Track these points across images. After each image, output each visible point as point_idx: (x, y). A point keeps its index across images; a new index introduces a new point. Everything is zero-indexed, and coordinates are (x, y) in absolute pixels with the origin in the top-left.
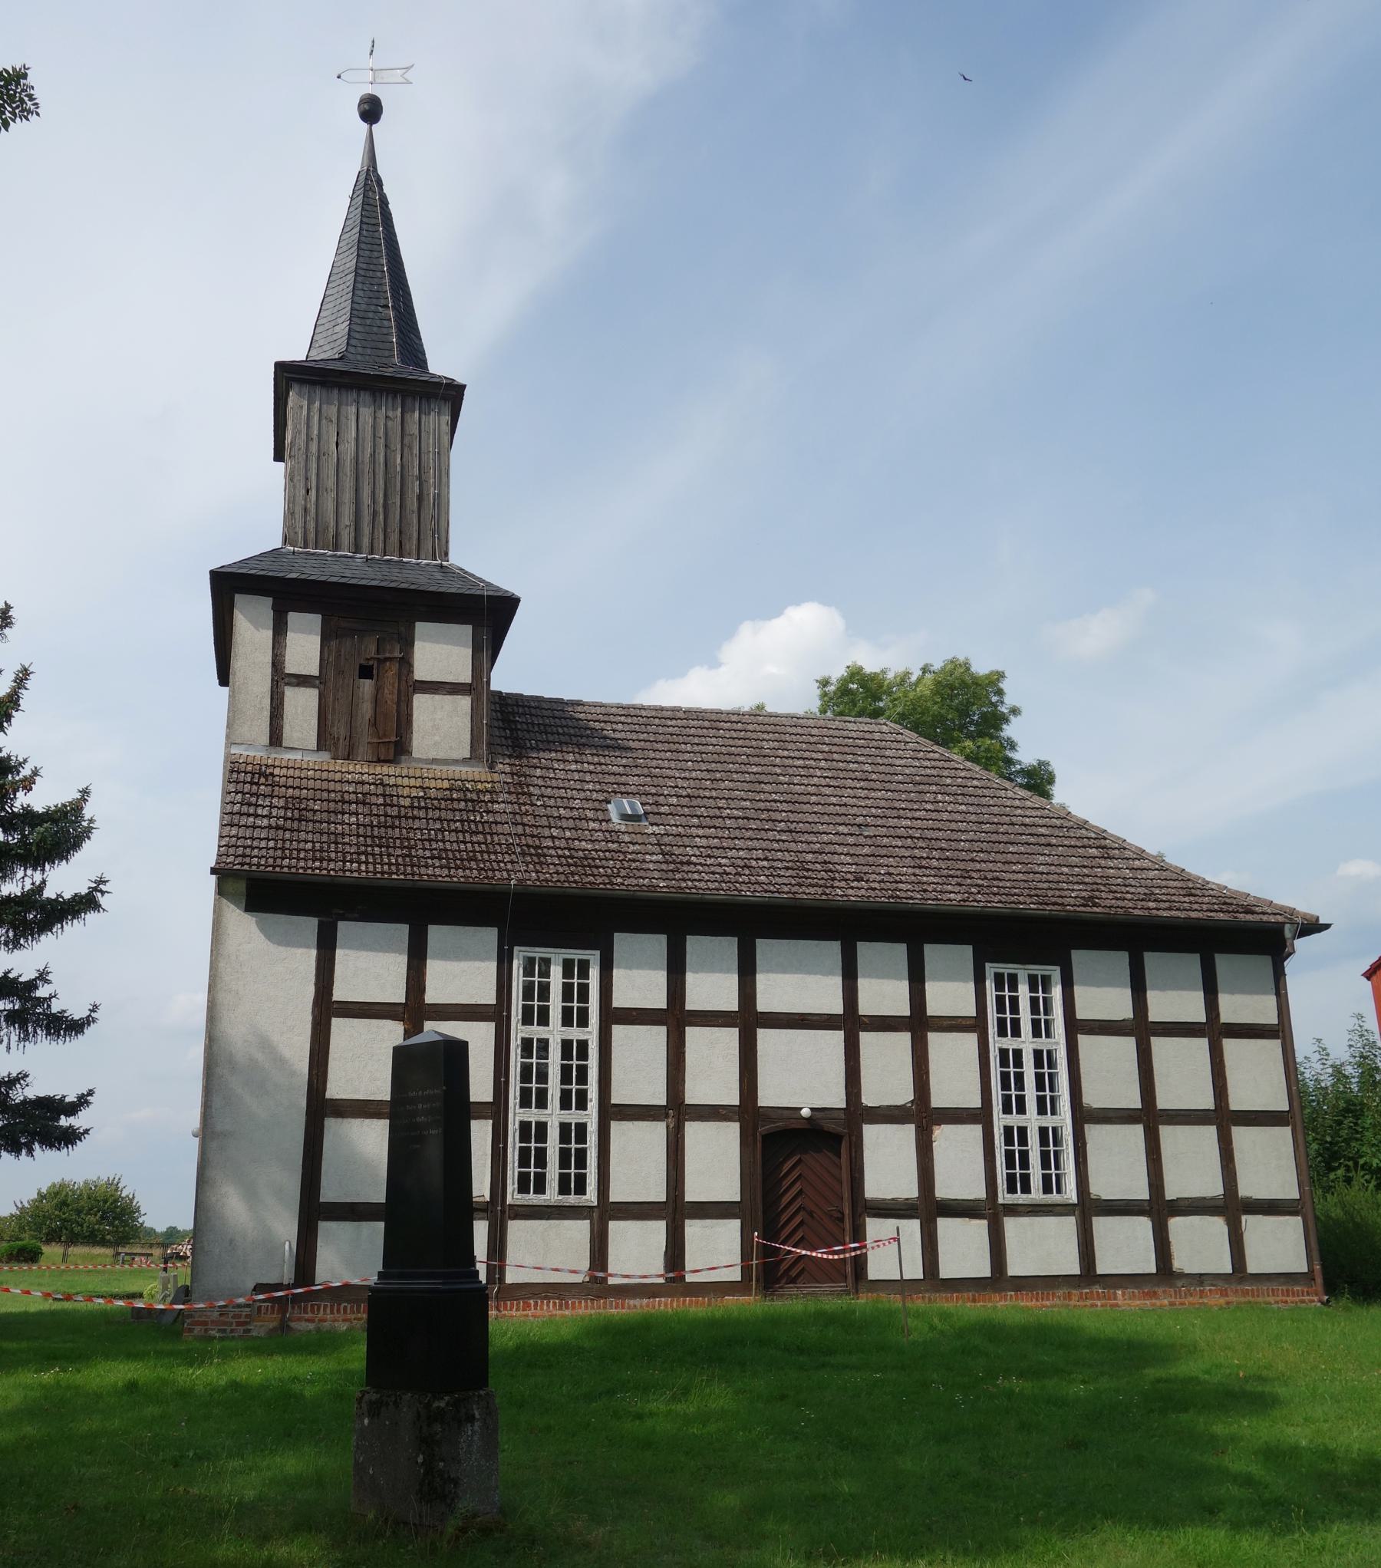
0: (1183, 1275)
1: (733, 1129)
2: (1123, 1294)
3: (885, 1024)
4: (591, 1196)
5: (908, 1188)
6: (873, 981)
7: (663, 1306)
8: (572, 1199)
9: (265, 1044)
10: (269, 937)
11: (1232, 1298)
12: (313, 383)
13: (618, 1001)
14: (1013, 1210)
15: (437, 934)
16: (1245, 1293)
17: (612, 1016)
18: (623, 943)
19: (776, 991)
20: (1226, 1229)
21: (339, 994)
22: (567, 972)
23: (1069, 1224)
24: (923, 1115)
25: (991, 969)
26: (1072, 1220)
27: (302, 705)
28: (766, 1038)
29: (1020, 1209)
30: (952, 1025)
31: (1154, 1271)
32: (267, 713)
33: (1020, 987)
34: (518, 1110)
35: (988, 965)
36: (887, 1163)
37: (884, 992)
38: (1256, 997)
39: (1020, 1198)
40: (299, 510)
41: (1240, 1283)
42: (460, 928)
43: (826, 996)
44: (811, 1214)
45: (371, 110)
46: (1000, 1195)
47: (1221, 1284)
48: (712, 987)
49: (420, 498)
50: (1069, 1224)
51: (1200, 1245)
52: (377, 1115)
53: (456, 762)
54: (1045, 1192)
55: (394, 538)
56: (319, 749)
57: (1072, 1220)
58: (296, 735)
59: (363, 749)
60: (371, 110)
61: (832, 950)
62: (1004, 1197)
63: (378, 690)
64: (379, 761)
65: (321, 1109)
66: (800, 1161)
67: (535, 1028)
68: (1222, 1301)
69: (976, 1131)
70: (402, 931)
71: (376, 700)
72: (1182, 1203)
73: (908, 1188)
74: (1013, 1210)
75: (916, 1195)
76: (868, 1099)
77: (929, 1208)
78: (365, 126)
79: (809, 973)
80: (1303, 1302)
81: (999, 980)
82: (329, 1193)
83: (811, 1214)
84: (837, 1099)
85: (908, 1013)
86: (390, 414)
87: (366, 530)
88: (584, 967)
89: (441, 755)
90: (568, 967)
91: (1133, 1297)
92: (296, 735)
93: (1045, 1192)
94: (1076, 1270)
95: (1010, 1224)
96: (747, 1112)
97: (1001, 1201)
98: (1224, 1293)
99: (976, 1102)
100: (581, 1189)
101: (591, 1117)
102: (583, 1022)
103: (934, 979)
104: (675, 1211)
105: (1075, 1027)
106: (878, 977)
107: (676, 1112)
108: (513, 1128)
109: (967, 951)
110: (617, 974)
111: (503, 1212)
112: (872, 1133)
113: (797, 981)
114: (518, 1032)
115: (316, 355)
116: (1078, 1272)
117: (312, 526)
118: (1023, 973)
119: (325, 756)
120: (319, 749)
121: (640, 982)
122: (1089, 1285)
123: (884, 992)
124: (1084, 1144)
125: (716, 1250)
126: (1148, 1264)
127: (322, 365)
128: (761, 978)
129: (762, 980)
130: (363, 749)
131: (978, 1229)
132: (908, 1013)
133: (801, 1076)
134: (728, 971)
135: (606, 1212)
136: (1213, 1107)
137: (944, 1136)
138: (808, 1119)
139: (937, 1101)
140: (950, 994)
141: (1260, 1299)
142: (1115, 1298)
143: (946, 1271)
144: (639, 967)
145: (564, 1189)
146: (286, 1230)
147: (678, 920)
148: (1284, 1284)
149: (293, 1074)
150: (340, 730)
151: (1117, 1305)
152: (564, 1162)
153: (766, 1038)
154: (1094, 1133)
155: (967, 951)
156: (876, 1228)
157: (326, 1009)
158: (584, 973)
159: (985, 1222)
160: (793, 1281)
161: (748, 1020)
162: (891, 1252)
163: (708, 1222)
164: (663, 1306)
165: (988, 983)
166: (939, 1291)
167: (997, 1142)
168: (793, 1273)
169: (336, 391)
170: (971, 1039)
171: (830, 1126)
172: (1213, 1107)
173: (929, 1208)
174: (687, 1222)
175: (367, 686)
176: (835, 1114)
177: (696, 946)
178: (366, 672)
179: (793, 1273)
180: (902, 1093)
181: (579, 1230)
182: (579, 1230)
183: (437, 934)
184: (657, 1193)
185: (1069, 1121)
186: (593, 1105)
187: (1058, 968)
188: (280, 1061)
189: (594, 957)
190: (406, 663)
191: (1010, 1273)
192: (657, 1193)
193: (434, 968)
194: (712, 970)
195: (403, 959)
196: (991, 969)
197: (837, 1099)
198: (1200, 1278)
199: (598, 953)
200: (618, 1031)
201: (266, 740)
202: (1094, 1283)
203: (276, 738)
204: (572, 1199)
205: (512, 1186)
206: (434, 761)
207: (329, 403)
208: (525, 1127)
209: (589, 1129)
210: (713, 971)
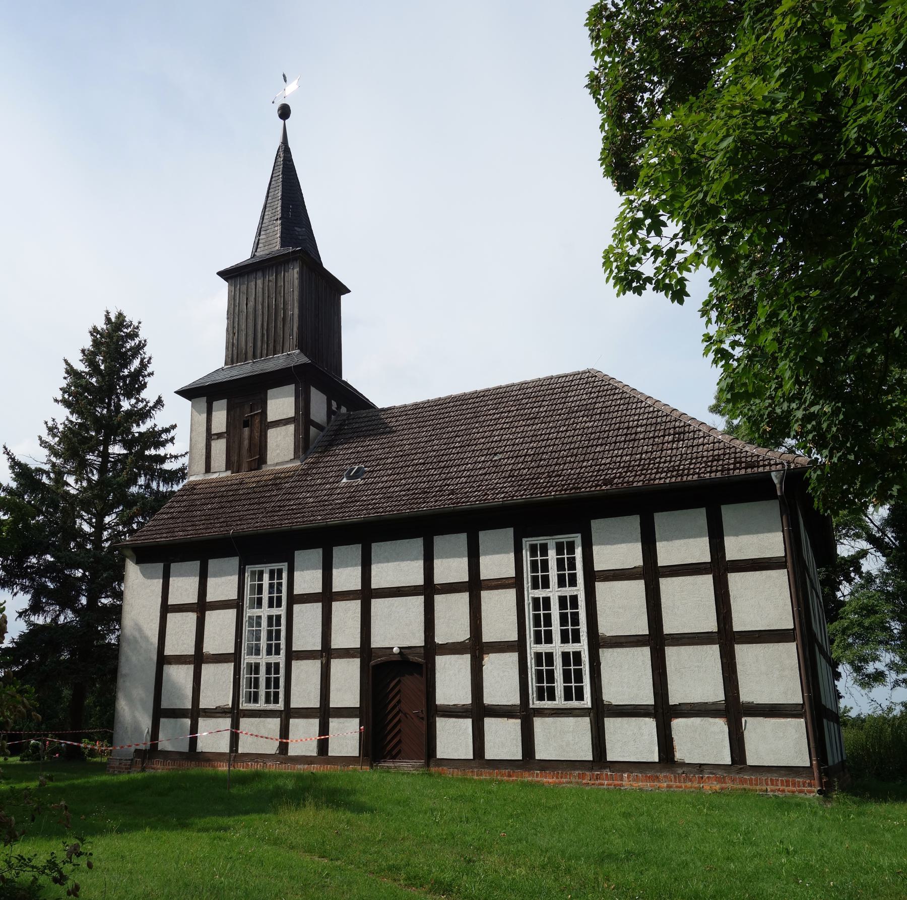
0: (683, 764)
1: (357, 662)
2: (628, 777)
3: (452, 588)
4: (280, 706)
5: (464, 697)
6: (444, 560)
7: (315, 768)
8: (574, 704)
9: (140, 630)
10: (144, 575)
11: (729, 785)
12: (236, 276)
13: (297, 591)
14: (542, 713)
15: (660, 519)
16: (743, 781)
17: (294, 600)
18: (300, 556)
19: (385, 574)
20: (726, 729)
21: (171, 601)
22: (559, 551)
23: (585, 723)
24: (476, 648)
25: (527, 542)
26: (587, 720)
27: (219, 448)
28: (735, 580)
29: (546, 712)
30: (499, 584)
31: (657, 760)
32: (204, 457)
33: (550, 552)
34: (532, 645)
35: (524, 540)
36: (452, 681)
37: (451, 568)
38: (761, 536)
39: (547, 704)
40: (230, 346)
41: (738, 773)
42: (618, 519)
43: (697, 550)
44: (405, 714)
45: (285, 112)
46: (531, 702)
47: (720, 773)
48: (347, 577)
49: (284, 319)
50: (585, 722)
51: (702, 742)
52: (353, 657)
53: (287, 462)
54: (566, 700)
55: (271, 346)
56: (227, 470)
57: (587, 720)
58: (216, 465)
59: (245, 466)
60: (285, 112)
61: (634, 523)
62: (280, 706)
63: (251, 431)
64: (251, 470)
65: (163, 660)
66: (399, 681)
67: (255, 610)
68: (717, 787)
69: (514, 657)
70: (463, 538)
71: (251, 438)
72: (684, 708)
73: (464, 697)
74: (542, 713)
75: (470, 702)
76: (439, 639)
77: (478, 711)
78: (282, 121)
79: (403, 560)
80: (801, 792)
81: (533, 550)
82: (165, 705)
83: (405, 714)
84: (417, 639)
85: (467, 579)
86: (271, 278)
87: (259, 343)
88: (571, 548)
89: (280, 460)
90: (559, 549)
91: (636, 779)
92: (216, 465)
93: (566, 700)
94: (519, 756)
95: (539, 724)
96: (365, 652)
97: (531, 706)
98: (721, 780)
99: (514, 637)
100: (580, 697)
101: (281, 659)
102: (573, 583)
103: (486, 554)
104: (325, 713)
105: (592, 577)
106: (447, 557)
107: (327, 653)
108: (243, 666)
109: (510, 531)
110: (297, 574)
111: (238, 713)
112: (441, 661)
113: (397, 568)
114: (531, 594)
115: (262, 252)
116: (591, 759)
117: (235, 352)
118: (551, 543)
119: (229, 473)
120: (227, 470)
121: (308, 580)
122: (740, 771)
123: (451, 568)
124: (599, 664)
125: (346, 737)
126: (467, 753)
127: (268, 257)
128: (596, 549)
129: (438, 563)
130: (245, 466)
131: (514, 726)
132: (467, 579)
133: (397, 627)
134: (507, 552)
135: (288, 714)
136: (716, 630)
137: (491, 662)
138: (400, 653)
139: (487, 637)
140: (497, 563)
141: (758, 787)
142: (622, 780)
143: (489, 754)
144: (308, 569)
145: (568, 697)
146: (146, 723)
147: (326, 539)
148: (785, 775)
149: (152, 644)
150: (235, 458)
151: (621, 785)
152: (567, 678)
153: (735, 580)
154: (607, 656)
155: (510, 531)
156: (442, 724)
157: (166, 609)
158: (571, 550)
159: (519, 721)
160: (394, 757)
161: (719, 568)
162: (453, 739)
163: (342, 720)
164: (315, 768)
165: (524, 552)
166: (484, 768)
167: (529, 664)
168: (394, 753)
169: (260, 274)
170: (510, 595)
171: (412, 658)
172: (716, 630)
173: (478, 711)
174: (330, 719)
175: (246, 431)
176: (418, 650)
177: (485, 537)
178: (246, 424)
179: (394, 753)
180: (462, 634)
181: (274, 724)
182: (274, 724)
183: (660, 519)
184: (315, 703)
185: (586, 647)
186: (283, 652)
187: (579, 535)
188: (146, 639)
189: (284, 566)
190: (264, 413)
191: (537, 758)
192: (315, 703)
193: (375, 569)
194: (347, 566)
195: (197, 579)
196: (527, 542)
197: (417, 639)
198: (701, 768)
199: (579, 535)
200: (601, 587)
201: (203, 470)
202: (605, 768)
203: (208, 469)
204: (574, 704)
205: (242, 699)
206: (277, 464)
207: (244, 284)
208: (538, 656)
209: (579, 599)
210: (347, 567)
